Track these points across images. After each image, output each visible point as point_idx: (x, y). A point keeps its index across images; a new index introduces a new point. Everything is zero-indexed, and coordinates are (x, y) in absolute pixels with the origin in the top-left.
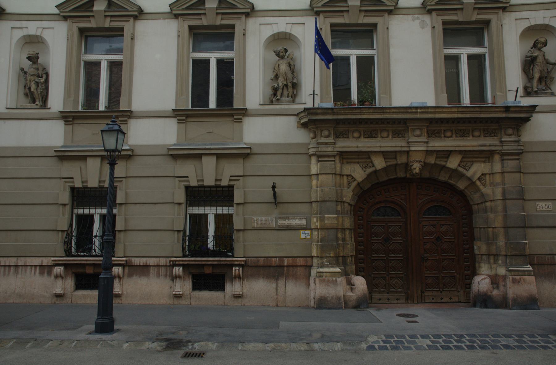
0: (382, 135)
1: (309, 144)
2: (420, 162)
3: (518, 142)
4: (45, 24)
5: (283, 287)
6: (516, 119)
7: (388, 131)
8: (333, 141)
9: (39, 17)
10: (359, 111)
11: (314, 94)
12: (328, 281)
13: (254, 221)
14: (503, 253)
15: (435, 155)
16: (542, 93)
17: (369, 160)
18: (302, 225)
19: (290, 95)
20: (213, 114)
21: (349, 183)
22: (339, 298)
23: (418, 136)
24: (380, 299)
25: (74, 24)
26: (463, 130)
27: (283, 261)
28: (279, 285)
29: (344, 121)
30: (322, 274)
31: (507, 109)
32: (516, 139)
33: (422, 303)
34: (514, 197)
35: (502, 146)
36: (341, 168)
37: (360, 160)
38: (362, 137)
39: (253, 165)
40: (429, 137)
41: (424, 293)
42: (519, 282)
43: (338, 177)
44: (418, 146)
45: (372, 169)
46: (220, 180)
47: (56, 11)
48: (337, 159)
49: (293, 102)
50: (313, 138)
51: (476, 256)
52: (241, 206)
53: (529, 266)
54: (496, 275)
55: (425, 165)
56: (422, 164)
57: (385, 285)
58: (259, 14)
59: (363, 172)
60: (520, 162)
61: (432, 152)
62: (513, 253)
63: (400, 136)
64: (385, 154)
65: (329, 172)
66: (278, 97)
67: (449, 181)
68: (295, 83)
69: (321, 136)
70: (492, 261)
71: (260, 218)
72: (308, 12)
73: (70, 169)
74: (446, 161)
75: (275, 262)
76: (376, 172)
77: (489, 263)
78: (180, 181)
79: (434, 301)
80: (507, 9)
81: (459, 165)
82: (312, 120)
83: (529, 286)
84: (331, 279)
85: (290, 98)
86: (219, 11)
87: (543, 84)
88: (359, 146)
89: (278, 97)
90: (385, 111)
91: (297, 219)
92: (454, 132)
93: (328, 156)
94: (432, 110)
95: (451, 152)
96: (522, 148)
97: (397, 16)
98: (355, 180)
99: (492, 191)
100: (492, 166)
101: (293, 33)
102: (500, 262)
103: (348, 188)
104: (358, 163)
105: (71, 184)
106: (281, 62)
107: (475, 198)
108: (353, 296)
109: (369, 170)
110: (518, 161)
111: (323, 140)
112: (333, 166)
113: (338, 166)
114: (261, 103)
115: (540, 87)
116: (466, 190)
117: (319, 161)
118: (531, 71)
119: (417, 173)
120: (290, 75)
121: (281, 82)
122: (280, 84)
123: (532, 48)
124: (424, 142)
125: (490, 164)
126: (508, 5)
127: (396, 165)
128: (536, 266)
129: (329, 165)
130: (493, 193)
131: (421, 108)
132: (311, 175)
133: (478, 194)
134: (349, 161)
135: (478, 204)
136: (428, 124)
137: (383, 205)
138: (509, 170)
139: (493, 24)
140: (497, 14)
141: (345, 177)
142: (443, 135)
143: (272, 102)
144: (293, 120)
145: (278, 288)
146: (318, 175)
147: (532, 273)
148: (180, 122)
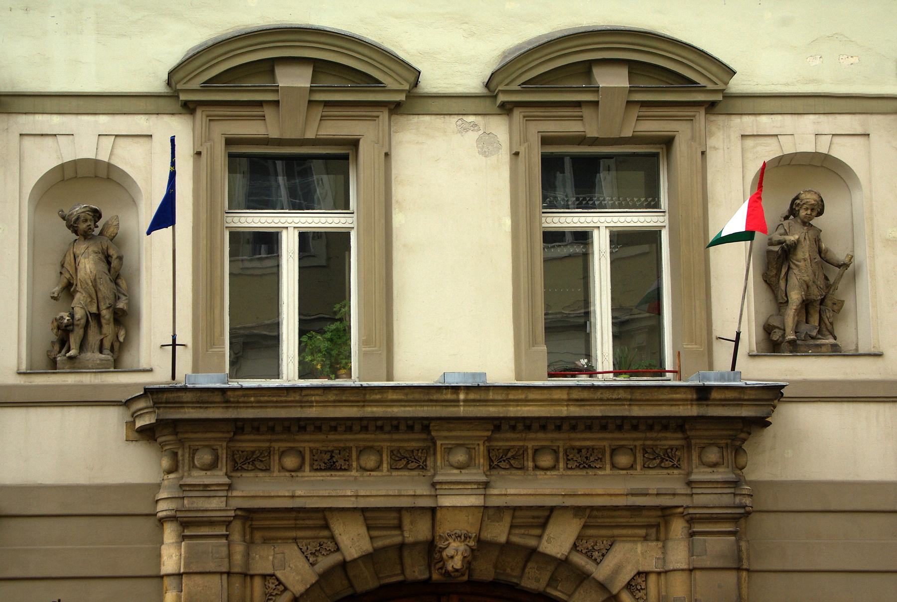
0: (363, 463)
1: (158, 486)
2: (467, 537)
3: (735, 484)
6: (738, 420)
7: (380, 452)
8: (226, 480)
10: (298, 398)
11: (174, 345)
15: (507, 519)
16: (809, 347)
17: (325, 533)
19: (107, 344)
23: (460, 467)
31: (703, 393)
32: (731, 477)
35: (692, 495)
36: (247, 555)
37: (300, 534)
38: (307, 468)
40: (492, 467)
43: (237, 582)
44: (460, 497)
45: (336, 558)
48: (237, 526)
49: (116, 365)
50: (169, 472)
55: (482, 546)
56: (472, 543)
58: (436, 105)
59: (307, 565)
60: (738, 541)
61: (500, 510)
63: (414, 465)
65: (211, 567)
66: (72, 353)
68: (122, 310)
69: (193, 466)
72: (162, 101)
74: (540, 537)
76: (344, 565)
80: (717, 109)
81: (575, 547)
82: (168, 420)
85: (107, 356)
87: (815, 320)
88: (298, 493)
89: (72, 353)
90: (368, 397)
92: (561, 455)
93: (211, 523)
94: (498, 397)
95: (552, 509)
96: (747, 501)
97: (415, 119)
98: (286, 589)
101: (115, 162)
104: (295, 540)
106: (81, 248)
109: (326, 562)
111: (198, 477)
112: (224, 550)
113: (239, 549)
114: (23, 368)
115: (804, 327)
117: (184, 538)
118: (782, 283)
119: (457, 570)
120: (106, 289)
121: (80, 306)
122: (79, 314)
123: (786, 218)
124: (478, 483)
125: (660, 544)
126: (718, 97)
127: (401, 547)
129: (214, 550)
131: (468, 388)
132: (162, 577)
134: (268, 534)
136: (489, 433)
138: (708, 564)
139: (681, 147)
140: (691, 119)
141: (258, 582)
142: (531, 464)
143: (53, 366)
144: (112, 420)
146: (180, 575)
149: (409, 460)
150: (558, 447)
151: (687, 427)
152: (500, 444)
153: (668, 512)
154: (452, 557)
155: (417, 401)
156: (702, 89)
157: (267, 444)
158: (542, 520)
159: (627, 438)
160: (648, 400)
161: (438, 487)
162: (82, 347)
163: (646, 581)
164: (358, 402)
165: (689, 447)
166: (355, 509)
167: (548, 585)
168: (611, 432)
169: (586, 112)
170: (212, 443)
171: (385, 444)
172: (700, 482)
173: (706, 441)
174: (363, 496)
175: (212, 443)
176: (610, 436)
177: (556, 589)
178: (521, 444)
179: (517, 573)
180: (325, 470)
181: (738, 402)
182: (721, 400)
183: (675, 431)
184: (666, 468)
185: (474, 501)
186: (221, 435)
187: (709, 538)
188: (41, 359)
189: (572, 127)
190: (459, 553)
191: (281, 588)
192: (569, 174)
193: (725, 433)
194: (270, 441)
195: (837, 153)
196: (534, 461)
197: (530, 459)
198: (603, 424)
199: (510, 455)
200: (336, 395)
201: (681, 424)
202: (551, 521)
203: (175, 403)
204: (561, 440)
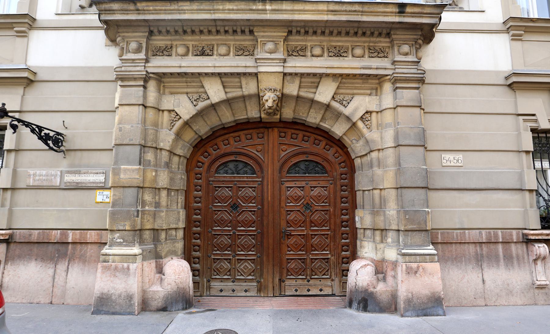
5: (64, 274)
12: (116, 268)
13: (30, 175)
14: (394, 227)
17: (202, 90)
18: (98, 183)
21: (172, 123)
22: (130, 297)
24: (221, 291)
26: (339, 46)
27: (67, 236)
28: (58, 271)
30: (107, 258)
32: (416, 60)
33: (281, 295)
34: (412, 143)
36: (159, 100)
37: (189, 90)
38: (190, 54)
41: (284, 281)
42: (416, 272)
51: (358, 231)
53: (431, 247)
54: (383, 261)
55: (283, 98)
56: (278, 94)
57: (229, 271)
59: (191, 106)
60: (420, 93)
62: (410, 227)
63: (247, 53)
67: (321, 124)
70: (378, 238)
71: (38, 172)
75: (56, 236)
77: (374, 241)
79: (298, 293)
83: (431, 278)
84: (120, 265)
88: (183, 65)
91: (91, 173)
92: (325, 49)
100: (380, 101)
102: (389, 240)
103: (170, 130)
105: (534, 125)
107: (357, 148)
108: (159, 291)
109: (201, 105)
110: (417, 91)
112: (141, 93)
116: (345, 137)
124: (280, 59)
125: (378, 97)
128: (440, 246)
130: (382, 138)
133: (361, 142)
135: (361, 157)
137: (251, 162)
138: (405, 104)
141: (166, 113)
142: (309, 54)
145: (56, 276)
147: (436, 257)
150: (324, 46)
151: (392, 33)
152: (293, 43)
153: (382, 79)
154: (267, 101)
155: (242, 10)
157: (169, 43)
158: (316, 85)
160: (371, 12)
161: (258, 61)
163: (370, 116)
164: (210, 10)
165: (393, 46)
166: (213, 74)
167: (321, 121)
168: (351, 37)
170: (138, 39)
171: (232, 43)
173: (402, 42)
174: (218, 67)
175: (138, 39)
176: (350, 39)
177: (325, 123)
178: (304, 43)
179: (305, 115)
180: (200, 55)
182: (411, 13)
183: (385, 37)
184: (380, 57)
185: (280, 69)
186: (141, 34)
187: (404, 90)
190: (271, 98)
191: (178, 117)
193: (412, 37)
194: (171, 40)
196: (311, 52)
197: (309, 51)
199: (298, 49)
200: (198, 6)
202: (321, 83)
203: (109, 10)
204: (325, 40)
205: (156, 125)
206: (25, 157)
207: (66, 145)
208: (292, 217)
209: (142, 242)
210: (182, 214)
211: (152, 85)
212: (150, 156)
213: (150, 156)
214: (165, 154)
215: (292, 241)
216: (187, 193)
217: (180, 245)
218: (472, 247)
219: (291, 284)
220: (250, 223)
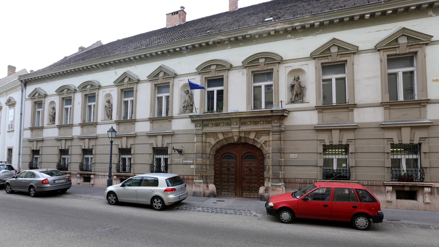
4: (111, 89)
6: (282, 116)
9: (293, 61)
15: (244, 133)
20: (401, 104)
22: (201, 193)
25: (319, 61)
29: (205, 120)
33: (242, 197)
36: (206, 139)
39: (360, 134)
46: (342, 142)
47: (147, 79)
52: (353, 154)
55: (240, 138)
58: (235, 68)
64: (223, 133)
69: (233, 125)
73: (152, 141)
78: (388, 141)
81: (255, 137)
86: (339, 53)
99: (268, 150)
105: (324, 143)
108: (207, 192)
109: (217, 140)
126: (429, 42)
139: (419, 54)
140: (421, 47)
148: (319, 112)
149: (229, 124)
156: (277, 60)
159: (262, 119)
162: (186, 110)
169: (258, 66)
172: (275, 125)
181: (278, 112)
185: (238, 130)
188: (182, 111)
189: (326, 61)
192: (257, 76)
195: (302, 68)
198: (257, 117)
201: (270, 116)
205: (205, 147)
206: (173, 155)
207: (183, 152)
208: (245, 173)
209: (203, 179)
210: (213, 172)
211: (204, 136)
212: (204, 156)
213: (204, 156)
214: (208, 155)
215: (245, 180)
216: (215, 165)
217: (213, 181)
218: (298, 184)
219: (245, 194)
220: (233, 175)
